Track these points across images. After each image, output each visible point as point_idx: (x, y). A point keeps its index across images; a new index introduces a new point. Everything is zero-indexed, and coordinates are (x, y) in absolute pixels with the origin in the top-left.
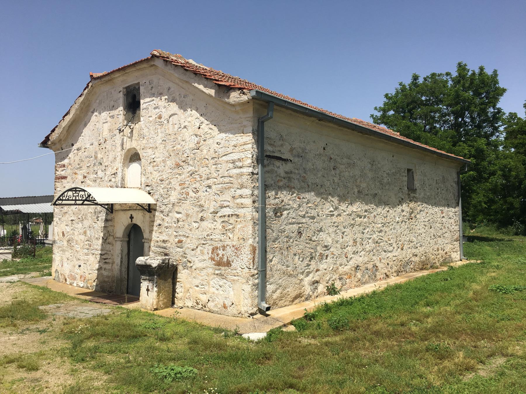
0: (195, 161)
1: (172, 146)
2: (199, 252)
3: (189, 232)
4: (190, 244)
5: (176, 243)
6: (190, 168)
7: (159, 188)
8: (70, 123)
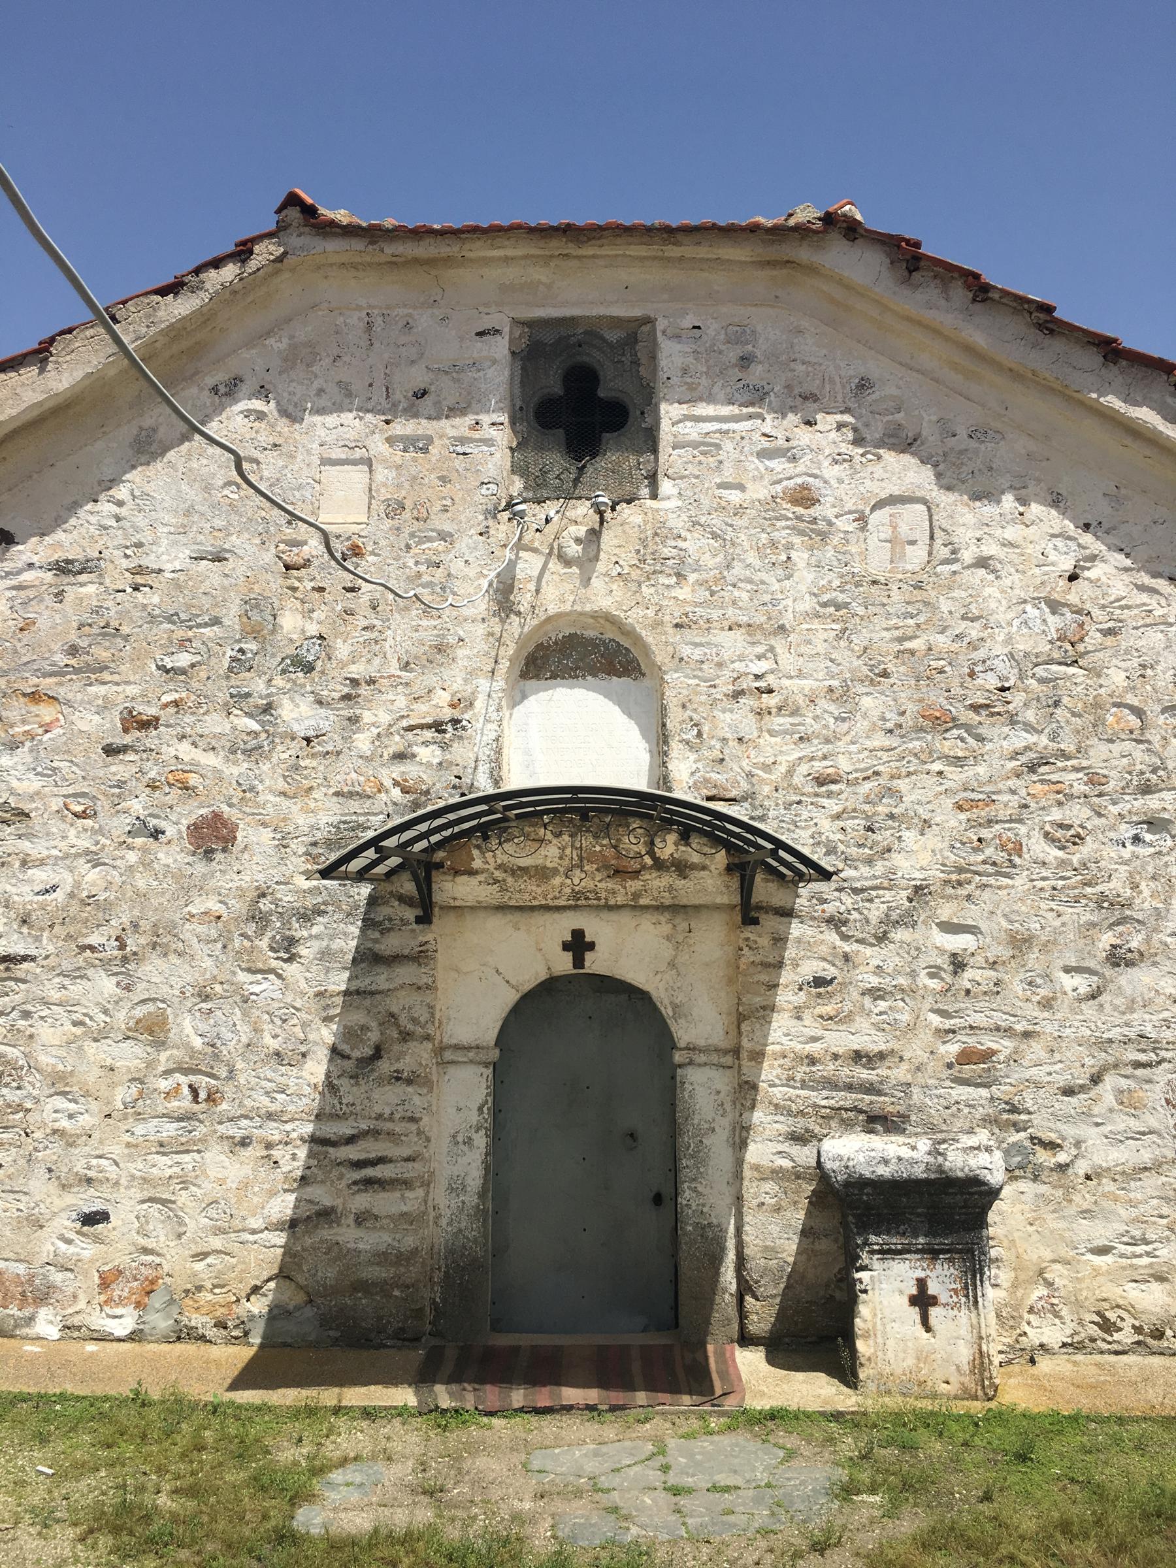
0: (1058, 711)
1: (898, 633)
2: (1109, 1099)
3: (1032, 1011)
4: (1048, 1068)
5: (950, 1066)
6: (1021, 739)
7: (805, 815)
8: (35, 413)
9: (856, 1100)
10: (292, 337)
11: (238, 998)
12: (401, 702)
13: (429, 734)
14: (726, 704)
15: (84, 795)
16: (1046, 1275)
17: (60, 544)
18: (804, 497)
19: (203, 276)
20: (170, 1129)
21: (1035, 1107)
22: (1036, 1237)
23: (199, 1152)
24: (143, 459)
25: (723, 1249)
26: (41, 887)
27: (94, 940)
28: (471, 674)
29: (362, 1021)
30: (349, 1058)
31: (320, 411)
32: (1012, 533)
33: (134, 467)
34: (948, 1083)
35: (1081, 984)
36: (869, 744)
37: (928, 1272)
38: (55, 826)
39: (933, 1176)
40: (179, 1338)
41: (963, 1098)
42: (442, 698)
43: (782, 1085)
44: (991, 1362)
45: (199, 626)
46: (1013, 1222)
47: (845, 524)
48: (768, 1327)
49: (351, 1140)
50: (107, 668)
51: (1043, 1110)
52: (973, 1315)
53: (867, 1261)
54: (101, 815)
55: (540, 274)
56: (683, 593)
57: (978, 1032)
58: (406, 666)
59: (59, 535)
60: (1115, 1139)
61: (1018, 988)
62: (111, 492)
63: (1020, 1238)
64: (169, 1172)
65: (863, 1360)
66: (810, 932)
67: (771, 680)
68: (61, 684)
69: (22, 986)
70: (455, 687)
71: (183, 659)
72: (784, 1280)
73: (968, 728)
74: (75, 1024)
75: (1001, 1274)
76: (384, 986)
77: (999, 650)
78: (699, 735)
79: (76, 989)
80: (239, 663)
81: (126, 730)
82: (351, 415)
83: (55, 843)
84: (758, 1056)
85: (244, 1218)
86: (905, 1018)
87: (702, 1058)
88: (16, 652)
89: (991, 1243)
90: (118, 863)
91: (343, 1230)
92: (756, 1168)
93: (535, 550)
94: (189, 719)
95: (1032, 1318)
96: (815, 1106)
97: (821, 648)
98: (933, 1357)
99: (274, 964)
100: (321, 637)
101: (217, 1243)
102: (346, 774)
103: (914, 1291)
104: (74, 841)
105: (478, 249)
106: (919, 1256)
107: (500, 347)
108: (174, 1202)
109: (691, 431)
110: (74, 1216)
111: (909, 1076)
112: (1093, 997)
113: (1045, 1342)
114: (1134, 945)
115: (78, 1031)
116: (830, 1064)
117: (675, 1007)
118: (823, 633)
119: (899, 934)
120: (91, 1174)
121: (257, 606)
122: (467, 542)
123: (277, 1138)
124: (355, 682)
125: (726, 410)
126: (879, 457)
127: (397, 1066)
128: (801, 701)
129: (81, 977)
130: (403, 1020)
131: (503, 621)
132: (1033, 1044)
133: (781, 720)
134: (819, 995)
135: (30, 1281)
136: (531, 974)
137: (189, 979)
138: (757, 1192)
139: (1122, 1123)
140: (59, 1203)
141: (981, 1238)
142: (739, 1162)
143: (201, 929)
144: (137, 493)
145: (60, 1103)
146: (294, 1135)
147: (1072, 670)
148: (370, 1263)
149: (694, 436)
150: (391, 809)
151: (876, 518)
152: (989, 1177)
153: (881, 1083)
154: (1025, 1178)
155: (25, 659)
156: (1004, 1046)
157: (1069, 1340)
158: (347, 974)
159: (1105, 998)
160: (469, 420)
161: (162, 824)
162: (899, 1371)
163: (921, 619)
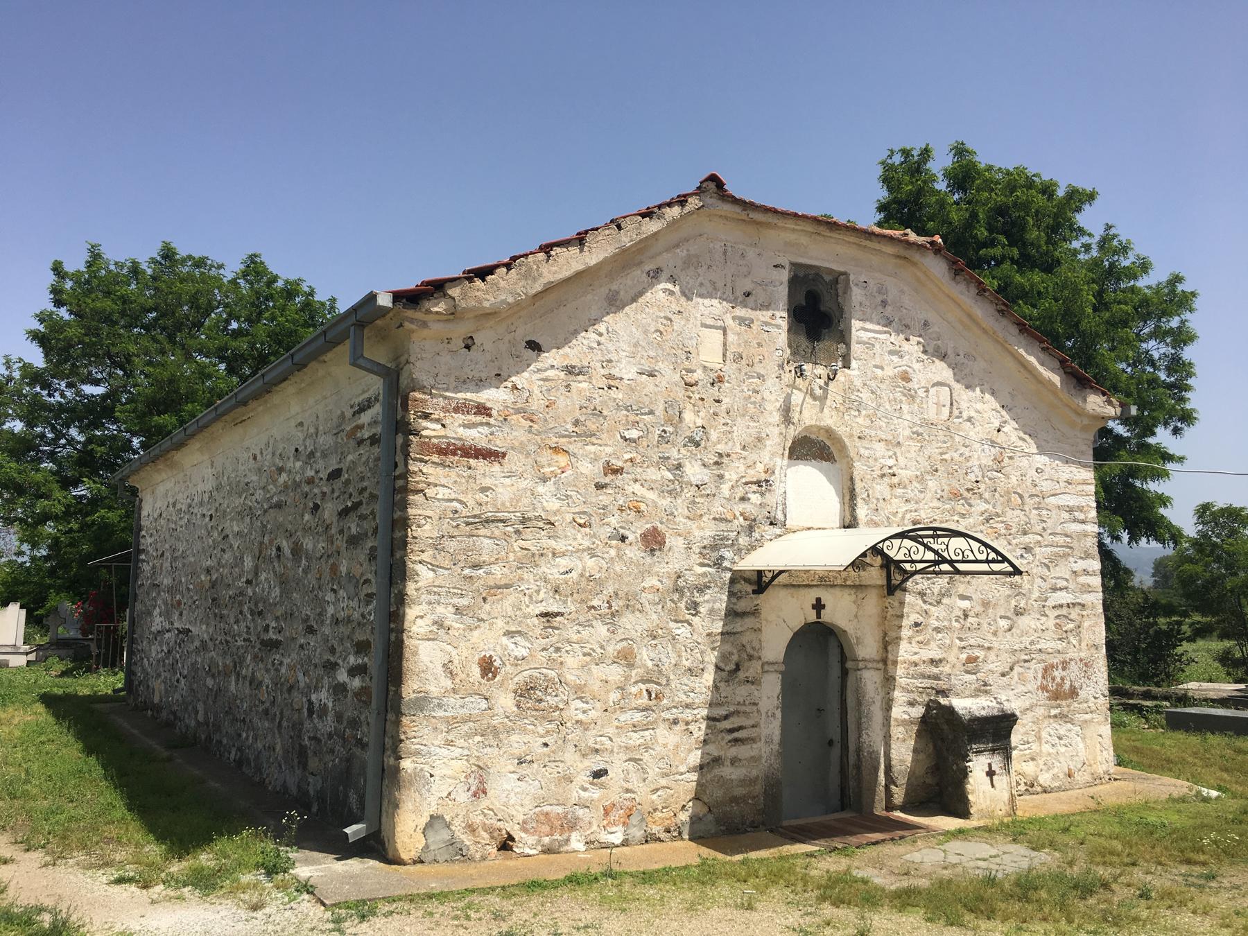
1: (941, 450)
3: (990, 637)
4: (996, 664)
10: (688, 250)
11: (670, 638)
12: (742, 468)
13: (755, 487)
14: (878, 480)
15: (584, 513)
17: (567, 355)
18: (906, 378)
19: (663, 210)
20: (638, 716)
23: (653, 729)
24: (613, 309)
25: (879, 763)
26: (564, 570)
27: (595, 603)
28: (773, 455)
29: (729, 650)
30: (724, 670)
31: (701, 296)
32: (979, 406)
33: (608, 313)
35: (1004, 624)
36: (932, 505)
38: (570, 531)
40: (646, 841)
42: (760, 467)
45: (642, 414)
47: (921, 393)
49: (726, 717)
50: (594, 435)
54: (594, 526)
55: (804, 240)
56: (860, 420)
58: (744, 448)
59: (566, 349)
60: (1018, 696)
61: (985, 625)
62: (596, 327)
64: (638, 742)
66: (913, 599)
67: (895, 470)
68: (571, 443)
69: (556, 632)
70: (765, 461)
71: (634, 434)
73: (965, 499)
74: (585, 655)
76: (739, 630)
77: (977, 463)
78: (868, 496)
79: (585, 633)
80: (664, 438)
81: (606, 475)
82: (717, 301)
83: (570, 542)
84: (895, 663)
85: (677, 766)
86: (948, 642)
87: (870, 665)
88: (546, 420)
90: (605, 556)
91: (724, 769)
92: (896, 720)
93: (800, 390)
94: (639, 470)
96: (917, 687)
97: (914, 455)
99: (688, 617)
100: (703, 427)
101: (663, 782)
102: (717, 508)
104: (581, 542)
105: (790, 224)
107: (785, 276)
108: (641, 760)
109: (864, 336)
110: (588, 774)
112: (1010, 630)
114: (1022, 605)
115: (588, 659)
117: (857, 638)
118: (914, 446)
119: (945, 600)
120: (597, 746)
121: (672, 405)
122: (771, 381)
123: (690, 718)
124: (720, 455)
125: (878, 328)
126: (933, 362)
127: (747, 674)
128: (907, 482)
129: (589, 626)
130: (749, 649)
131: (786, 427)
133: (899, 490)
134: (917, 631)
135: (565, 817)
136: (797, 624)
137: (645, 626)
138: (897, 732)
139: (1021, 689)
140: (581, 766)
143: (650, 597)
144: (610, 330)
145: (579, 704)
146: (699, 716)
147: (999, 475)
148: (738, 786)
149: (865, 339)
150: (740, 529)
151: (933, 391)
155: (551, 426)
156: (980, 654)
158: (722, 623)
159: (1014, 630)
160: (770, 313)
161: (626, 533)
163: (949, 444)
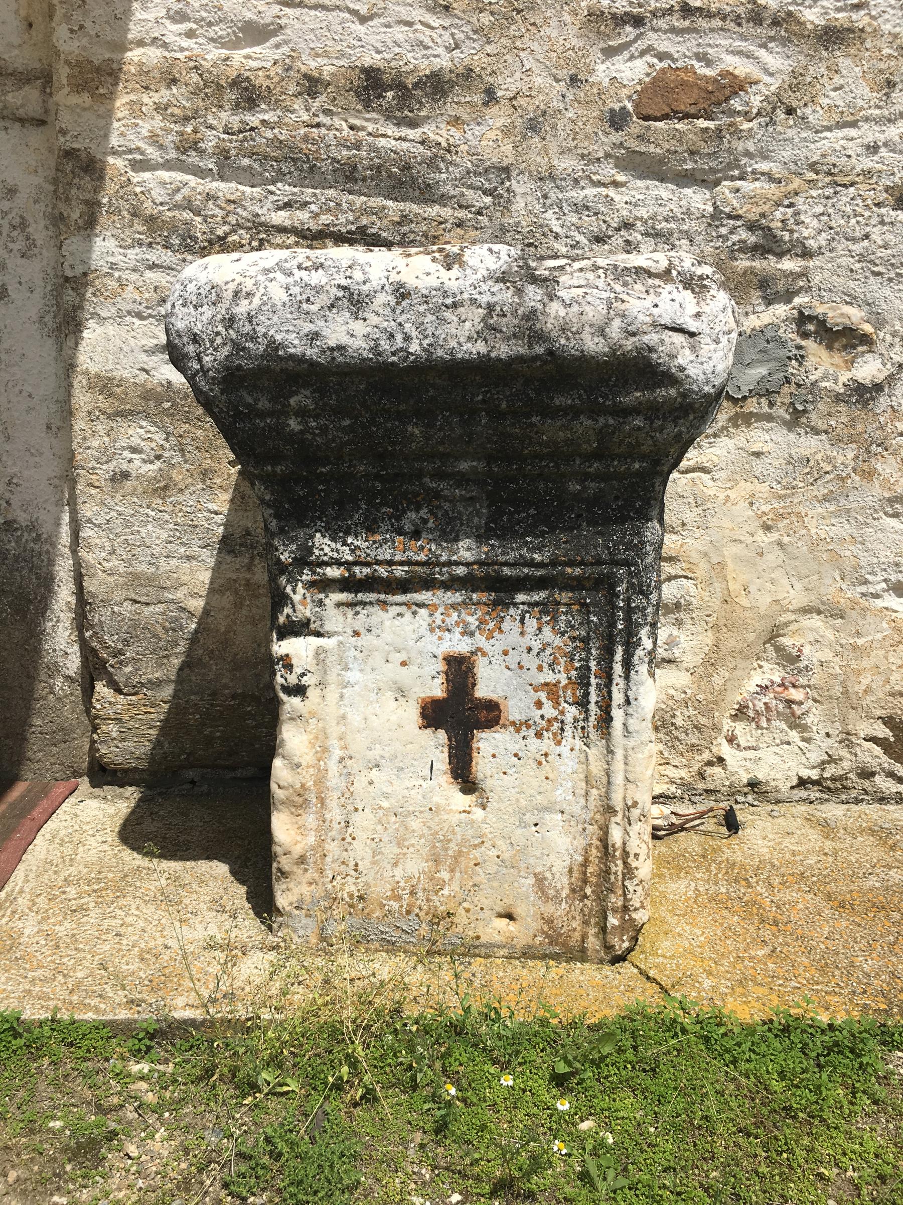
4: (869, 133)
5: (617, 120)
9: (364, 211)
16: (786, 641)
21: (823, 239)
22: (773, 557)
25: (47, 583)
34: (608, 171)
37: (480, 640)
39: (503, 350)
41: (643, 213)
43: (167, 165)
44: (629, 872)
46: (727, 523)
48: (146, 748)
51: (841, 246)
52: (595, 753)
53: (305, 611)
57: (703, 23)
63: (738, 559)
65: (285, 863)
72: (181, 649)
75: (682, 637)
89: (668, 569)
95: (740, 729)
98: (476, 854)
103: (437, 690)
106: (458, 597)
111: (508, 148)
113: (761, 776)
116: (298, 105)
132: (844, 63)
141: (639, 549)
142: (70, 367)
152: (685, 358)
153: (432, 163)
154: (769, 418)
157: (814, 774)
162: (380, 889)
